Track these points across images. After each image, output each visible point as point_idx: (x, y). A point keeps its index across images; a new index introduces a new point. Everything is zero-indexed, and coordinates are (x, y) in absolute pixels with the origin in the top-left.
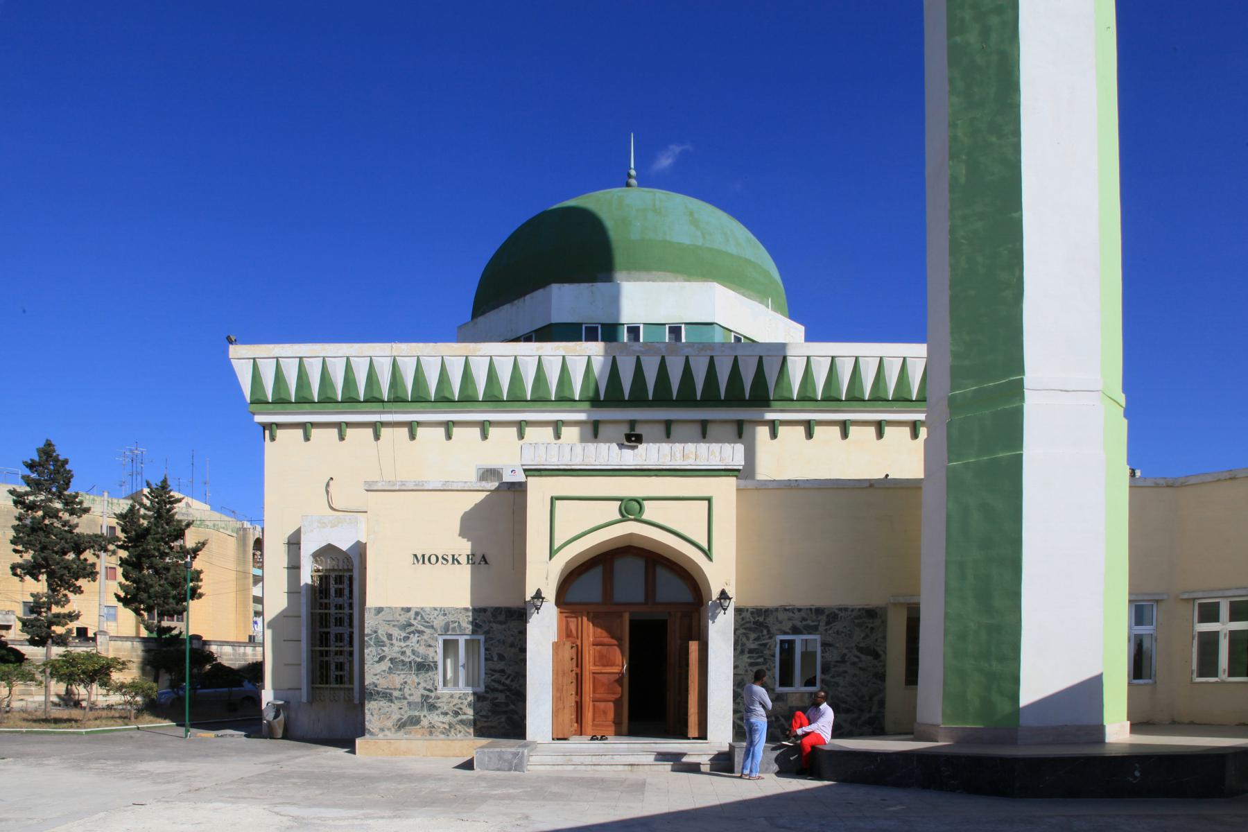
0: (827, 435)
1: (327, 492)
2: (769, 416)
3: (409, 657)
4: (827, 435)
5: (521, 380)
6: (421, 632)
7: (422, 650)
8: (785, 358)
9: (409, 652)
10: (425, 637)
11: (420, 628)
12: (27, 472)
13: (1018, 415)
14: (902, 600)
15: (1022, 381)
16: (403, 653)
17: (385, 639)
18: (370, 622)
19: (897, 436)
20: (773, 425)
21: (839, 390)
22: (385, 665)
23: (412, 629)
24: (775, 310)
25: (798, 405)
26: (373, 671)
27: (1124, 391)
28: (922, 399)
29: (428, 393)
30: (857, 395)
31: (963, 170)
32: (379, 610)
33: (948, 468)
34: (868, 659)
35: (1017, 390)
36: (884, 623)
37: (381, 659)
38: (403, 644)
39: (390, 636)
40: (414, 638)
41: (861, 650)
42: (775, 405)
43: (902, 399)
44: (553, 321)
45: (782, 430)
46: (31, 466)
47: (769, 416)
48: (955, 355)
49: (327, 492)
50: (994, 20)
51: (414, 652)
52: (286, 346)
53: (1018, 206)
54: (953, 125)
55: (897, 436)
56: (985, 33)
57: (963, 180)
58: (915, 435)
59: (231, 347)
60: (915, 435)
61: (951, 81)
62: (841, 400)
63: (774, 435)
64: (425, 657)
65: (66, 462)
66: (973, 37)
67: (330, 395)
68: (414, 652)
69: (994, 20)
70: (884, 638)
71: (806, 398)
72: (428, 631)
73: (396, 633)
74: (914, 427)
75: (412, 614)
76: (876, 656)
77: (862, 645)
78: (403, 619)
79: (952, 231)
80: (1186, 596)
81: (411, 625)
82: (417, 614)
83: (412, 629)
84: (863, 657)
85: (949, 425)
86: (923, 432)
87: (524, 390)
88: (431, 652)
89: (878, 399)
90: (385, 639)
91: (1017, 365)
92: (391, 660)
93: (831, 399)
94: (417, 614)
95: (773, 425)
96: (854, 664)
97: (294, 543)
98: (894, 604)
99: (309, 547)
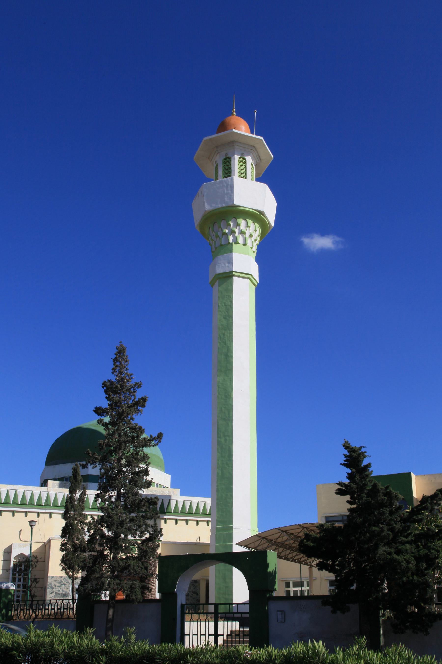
0: (182, 523)
1: (20, 535)
2: (165, 517)
3: (61, 592)
4: (182, 523)
5: (89, 502)
6: (65, 584)
7: (65, 590)
8: (170, 500)
9: (61, 591)
10: (66, 586)
11: (65, 583)
13: (231, 534)
14: (204, 578)
15: (232, 526)
16: (59, 591)
17: (54, 586)
18: (49, 581)
19: (203, 525)
22: (53, 595)
23: (62, 583)
24: (161, 470)
25: (174, 514)
26: (49, 597)
27: (258, 528)
29: (58, 504)
30: (191, 512)
31: (220, 472)
32: (53, 577)
33: (216, 546)
34: (195, 595)
35: (231, 528)
36: (199, 584)
37: (52, 593)
38: (59, 588)
39: (55, 586)
40: (63, 586)
41: (193, 592)
42: (167, 513)
47: (165, 517)
48: (218, 517)
49: (20, 535)
50: (228, 438)
51: (62, 591)
52: (12, 486)
53: (232, 484)
55: (203, 525)
56: (226, 440)
57: (220, 475)
58: (208, 525)
60: (208, 525)
61: (218, 449)
62: (187, 513)
63: (166, 523)
64: (66, 592)
65: (334, 612)
67: (25, 502)
68: (62, 591)
69: (228, 438)
70: (199, 589)
71: (176, 512)
72: (67, 584)
73: (58, 584)
74: (208, 522)
75: (63, 578)
76: (197, 594)
77: (193, 591)
78: (60, 580)
79: (217, 486)
80: (282, 580)
81: (62, 582)
82: (64, 578)
83: (62, 583)
84: (194, 595)
85: (216, 535)
86: (210, 523)
88: (68, 591)
90: (54, 586)
91: (231, 522)
92: (56, 593)
94: (64, 578)
95: (165, 520)
96: (191, 596)
98: (202, 579)
99: (14, 554)
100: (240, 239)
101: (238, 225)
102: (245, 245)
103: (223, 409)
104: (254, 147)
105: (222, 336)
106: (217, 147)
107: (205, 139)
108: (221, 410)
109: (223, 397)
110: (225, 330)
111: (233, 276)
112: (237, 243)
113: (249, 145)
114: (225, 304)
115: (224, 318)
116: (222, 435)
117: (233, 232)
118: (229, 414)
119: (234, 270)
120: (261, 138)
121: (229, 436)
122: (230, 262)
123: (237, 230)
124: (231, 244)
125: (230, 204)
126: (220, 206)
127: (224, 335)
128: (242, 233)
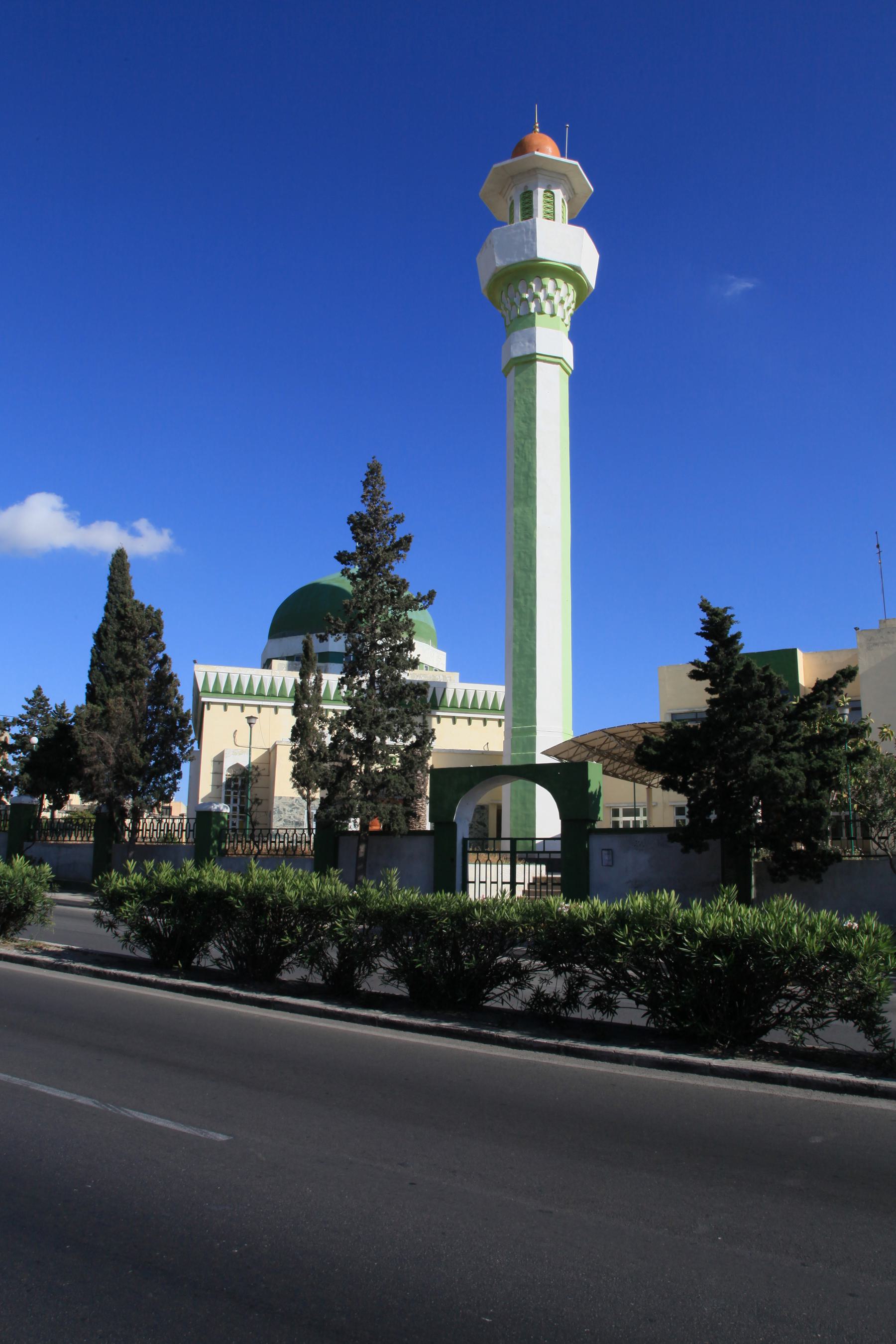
2: (438, 713)
3: (292, 819)
7: (298, 816)
12: (26, 704)
18: (276, 803)
20: (439, 718)
21: (468, 704)
22: (282, 823)
28: (503, 710)
31: (517, 648)
32: (280, 798)
33: (513, 730)
34: (481, 827)
35: (534, 731)
36: (488, 811)
39: (284, 810)
40: (295, 811)
42: (441, 709)
43: (494, 709)
44: (330, 650)
45: (442, 719)
46: (29, 702)
47: (438, 713)
48: (514, 714)
50: (529, 597)
52: (222, 667)
53: (535, 666)
54: (514, 630)
56: (526, 600)
58: (500, 725)
59: (196, 666)
60: (500, 725)
62: (469, 708)
63: (439, 722)
66: (522, 601)
69: (529, 597)
71: (453, 707)
73: (287, 808)
74: (500, 721)
76: (485, 826)
78: (290, 802)
79: (514, 668)
86: (503, 723)
87: (330, 695)
89: (484, 709)
91: (534, 721)
93: (464, 708)
95: (439, 718)
97: (219, 761)
99: (228, 764)
100: (547, 307)
101: (543, 287)
102: (553, 315)
103: (522, 554)
104: (565, 175)
105: (521, 449)
106: (512, 177)
107: (495, 166)
108: (519, 557)
109: (523, 537)
110: (525, 439)
111: (536, 360)
112: (541, 312)
113: (559, 174)
114: (524, 400)
115: (524, 422)
116: (520, 592)
117: (535, 297)
118: (531, 562)
119: (537, 352)
120: (576, 163)
121: (530, 595)
122: (532, 340)
123: (541, 295)
124: (533, 314)
125: (532, 257)
126: (516, 260)
127: (523, 446)
128: (549, 298)
